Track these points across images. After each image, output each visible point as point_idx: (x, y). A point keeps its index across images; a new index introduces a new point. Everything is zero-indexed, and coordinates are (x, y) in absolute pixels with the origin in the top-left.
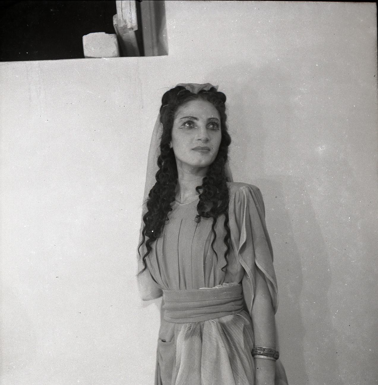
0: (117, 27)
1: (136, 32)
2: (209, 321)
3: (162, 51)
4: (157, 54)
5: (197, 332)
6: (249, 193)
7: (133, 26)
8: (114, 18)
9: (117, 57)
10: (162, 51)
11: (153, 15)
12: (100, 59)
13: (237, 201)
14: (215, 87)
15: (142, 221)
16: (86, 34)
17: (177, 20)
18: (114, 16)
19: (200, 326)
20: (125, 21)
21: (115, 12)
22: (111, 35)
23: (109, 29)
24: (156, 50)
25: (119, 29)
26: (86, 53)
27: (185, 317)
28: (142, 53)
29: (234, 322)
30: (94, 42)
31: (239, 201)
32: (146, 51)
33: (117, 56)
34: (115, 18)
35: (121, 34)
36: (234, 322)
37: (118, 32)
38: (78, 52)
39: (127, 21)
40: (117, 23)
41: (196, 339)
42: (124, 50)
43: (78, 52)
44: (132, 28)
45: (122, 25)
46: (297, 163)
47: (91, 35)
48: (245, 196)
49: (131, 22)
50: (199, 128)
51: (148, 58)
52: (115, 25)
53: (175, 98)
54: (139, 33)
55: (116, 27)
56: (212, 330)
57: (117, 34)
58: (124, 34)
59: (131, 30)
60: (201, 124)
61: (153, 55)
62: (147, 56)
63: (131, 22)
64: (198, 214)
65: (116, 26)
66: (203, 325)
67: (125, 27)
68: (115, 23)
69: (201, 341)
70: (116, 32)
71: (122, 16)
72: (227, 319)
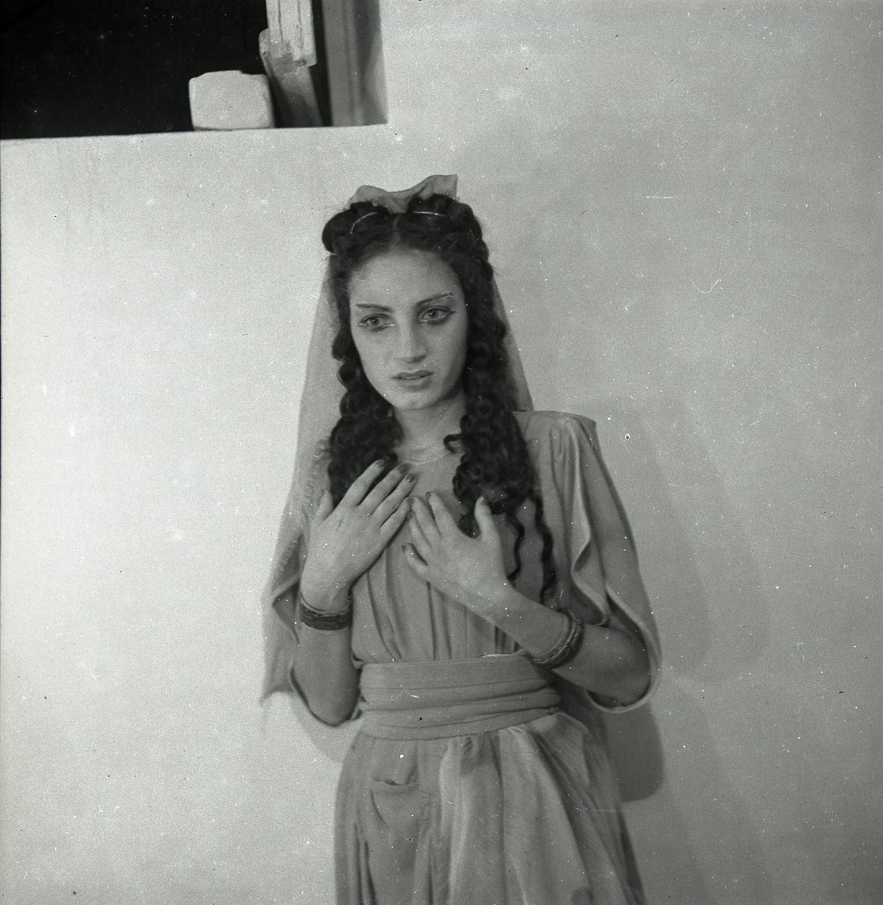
0: (269, 58)
1: (312, 69)
2: (509, 729)
3: (372, 114)
4: (360, 121)
5: (485, 756)
6: (582, 432)
7: (304, 56)
8: (261, 38)
9: (268, 127)
10: (372, 114)
11: (351, 29)
12: (228, 133)
13: (556, 451)
14: (356, 201)
15: (303, 567)
16: (197, 76)
17: (408, 44)
18: (261, 33)
19: (491, 742)
20: (288, 45)
21: (264, 24)
22: (255, 76)
23: (251, 63)
24: (359, 113)
25: (273, 63)
26: (197, 118)
27: (458, 721)
28: (327, 121)
29: (561, 728)
30: (215, 93)
31: (560, 451)
32: (336, 116)
33: (268, 125)
34: (264, 38)
35: (277, 74)
36: (561, 728)
37: (271, 70)
38: (180, 120)
39: (292, 44)
40: (269, 48)
41: (489, 769)
42: (283, 113)
43: (180, 120)
44: (303, 61)
45: (278, 54)
46: (674, 376)
47: (207, 76)
48: (574, 436)
49: (301, 47)
50: (397, 328)
51: (341, 129)
52: (264, 53)
53: (357, 234)
54: (320, 73)
55: (266, 58)
56: (518, 745)
57: (269, 73)
58: (286, 75)
59: (301, 66)
60: (402, 318)
61: (353, 124)
62: (339, 126)
63: (301, 47)
64: (465, 514)
65: (266, 55)
66: (497, 738)
67: (287, 59)
68: (263, 48)
69: (496, 774)
70: (267, 70)
71: (281, 32)
72: (544, 724)
